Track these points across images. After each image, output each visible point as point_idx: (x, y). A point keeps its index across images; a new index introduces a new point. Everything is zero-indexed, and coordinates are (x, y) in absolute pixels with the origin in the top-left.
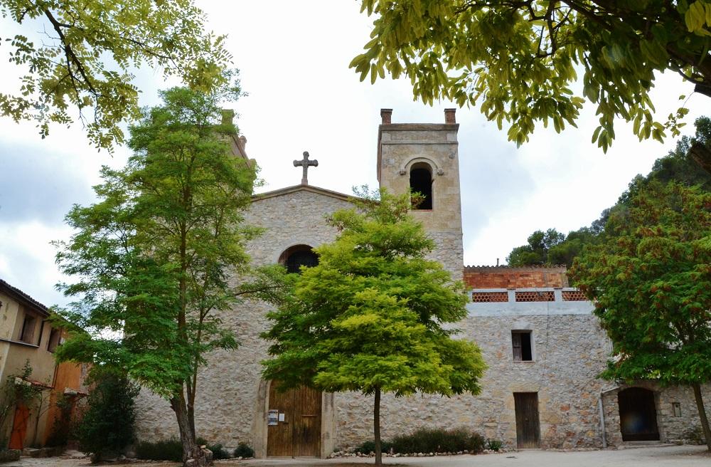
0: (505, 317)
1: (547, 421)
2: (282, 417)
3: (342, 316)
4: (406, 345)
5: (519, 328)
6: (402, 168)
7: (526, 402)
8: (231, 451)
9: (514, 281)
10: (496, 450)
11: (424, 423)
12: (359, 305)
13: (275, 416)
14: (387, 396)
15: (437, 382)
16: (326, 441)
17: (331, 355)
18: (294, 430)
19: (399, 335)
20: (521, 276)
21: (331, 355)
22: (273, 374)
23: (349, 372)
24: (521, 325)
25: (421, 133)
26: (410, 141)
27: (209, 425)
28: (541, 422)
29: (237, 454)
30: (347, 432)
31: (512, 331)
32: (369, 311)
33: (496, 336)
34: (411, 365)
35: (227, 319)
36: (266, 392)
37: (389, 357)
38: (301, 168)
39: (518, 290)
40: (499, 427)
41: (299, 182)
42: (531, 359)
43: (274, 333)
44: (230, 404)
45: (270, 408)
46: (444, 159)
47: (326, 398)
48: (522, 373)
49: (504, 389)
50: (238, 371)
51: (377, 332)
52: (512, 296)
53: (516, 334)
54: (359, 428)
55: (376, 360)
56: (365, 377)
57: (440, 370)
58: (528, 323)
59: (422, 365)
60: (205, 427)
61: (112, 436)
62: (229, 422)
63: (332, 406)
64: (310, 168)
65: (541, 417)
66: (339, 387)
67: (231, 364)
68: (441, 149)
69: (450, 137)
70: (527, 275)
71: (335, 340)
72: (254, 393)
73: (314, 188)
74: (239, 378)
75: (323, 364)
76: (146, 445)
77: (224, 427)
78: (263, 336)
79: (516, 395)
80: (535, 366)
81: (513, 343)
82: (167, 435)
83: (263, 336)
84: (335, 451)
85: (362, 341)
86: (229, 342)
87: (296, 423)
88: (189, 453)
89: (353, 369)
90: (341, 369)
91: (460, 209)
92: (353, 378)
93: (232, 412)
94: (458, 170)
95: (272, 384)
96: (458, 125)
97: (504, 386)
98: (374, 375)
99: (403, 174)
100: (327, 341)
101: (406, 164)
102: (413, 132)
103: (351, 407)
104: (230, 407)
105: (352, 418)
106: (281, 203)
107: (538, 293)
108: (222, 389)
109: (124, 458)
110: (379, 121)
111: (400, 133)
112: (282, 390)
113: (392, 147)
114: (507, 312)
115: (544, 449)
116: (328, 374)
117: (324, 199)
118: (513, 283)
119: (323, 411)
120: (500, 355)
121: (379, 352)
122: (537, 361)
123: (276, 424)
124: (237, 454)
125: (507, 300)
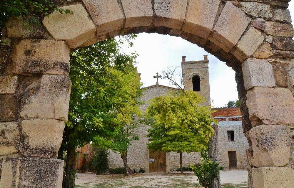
0: (225, 126)
1: (239, 161)
2: (153, 160)
3: (169, 131)
4: (188, 139)
5: (229, 130)
6: (190, 77)
7: (232, 155)
8: (138, 171)
9: (231, 112)
10: (222, 170)
11: (198, 161)
12: (174, 128)
13: (151, 160)
14: (184, 154)
15: (196, 149)
16: (167, 167)
17: (166, 142)
18: (157, 164)
19: (185, 136)
20: (234, 111)
21: (166, 142)
22: (150, 147)
23: (171, 147)
24: (230, 129)
25: (196, 64)
26: (192, 67)
27: (131, 163)
28: (237, 161)
29: (140, 172)
30: (174, 164)
31: (227, 131)
32: (177, 129)
33: (222, 133)
34: (189, 144)
35: (135, 131)
36: (148, 152)
37: (182, 142)
38: (156, 78)
39: (229, 117)
40: (223, 162)
41: (155, 84)
42: (234, 140)
43: (150, 135)
44: (137, 156)
45: (149, 157)
46: (204, 73)
47: (167, 154)
48: (231, 145)
49: (225, 150)
50: (139, 146)
51: (179, 136)
52: (227, 119)
53: (228, 132)
54: (178, 163)
55: (179, 143)
56: (176, 148)
57: (198, 145)
58: (233, 128)
59: (192, 144)
60: (129, 163)
61: (102, 167)
62: (137, 162)
63: (169, 156)
64: (159, 78)
65: (237, 160)
66: (169, 151)
67: (136, 144)
68: (203, 69)
69: (206, 65)
70: (235, 110)
71: (167, 138)
72: (144, 153)
73: (161, 85)
74: (140, 148)
75: (164, 145)
76: (112, 169)
77: (135, 163)
78: (147, 136)
79: (229, 152)
80: (236, 143)
81: (228, 135)
82: (118, 166)
83: (147, 136)
84: (170, 170)
85: (176, 138)
86: (137, 138)
87: (158, 162)
88: (127, 170)
89: (172, 146)
90: (169, 146)
91: (209, 90)
92: (173, 149)
93: (138, 159)
94: (208, 77)
95: (150, 150)
96: (208, 61)
97: (225, 149)
98: (178, 147)
99: (190, 79)
100: (165, 138)
101: (191, 75)
102: (193, 64)
103: (175, 157)
104: (137, 157)
105: (176, 160)
106: (150, 91)
107: (236, 118)
108: (134, 152)
109: (106, 173)
110: (181, 60)
111: (188, 65)
112: (153, 152)
113: (186, 70)
114: (226, 125)
115: (238, 170)
116: (165, 148)
117: (164, 89)
118: (231, 113)
119: (166, 158)
120: (223, 139)
121: (180, 141)
122: (236, 141)
123: (151, 162)
124: (140, 172)
125: (226, 121)
